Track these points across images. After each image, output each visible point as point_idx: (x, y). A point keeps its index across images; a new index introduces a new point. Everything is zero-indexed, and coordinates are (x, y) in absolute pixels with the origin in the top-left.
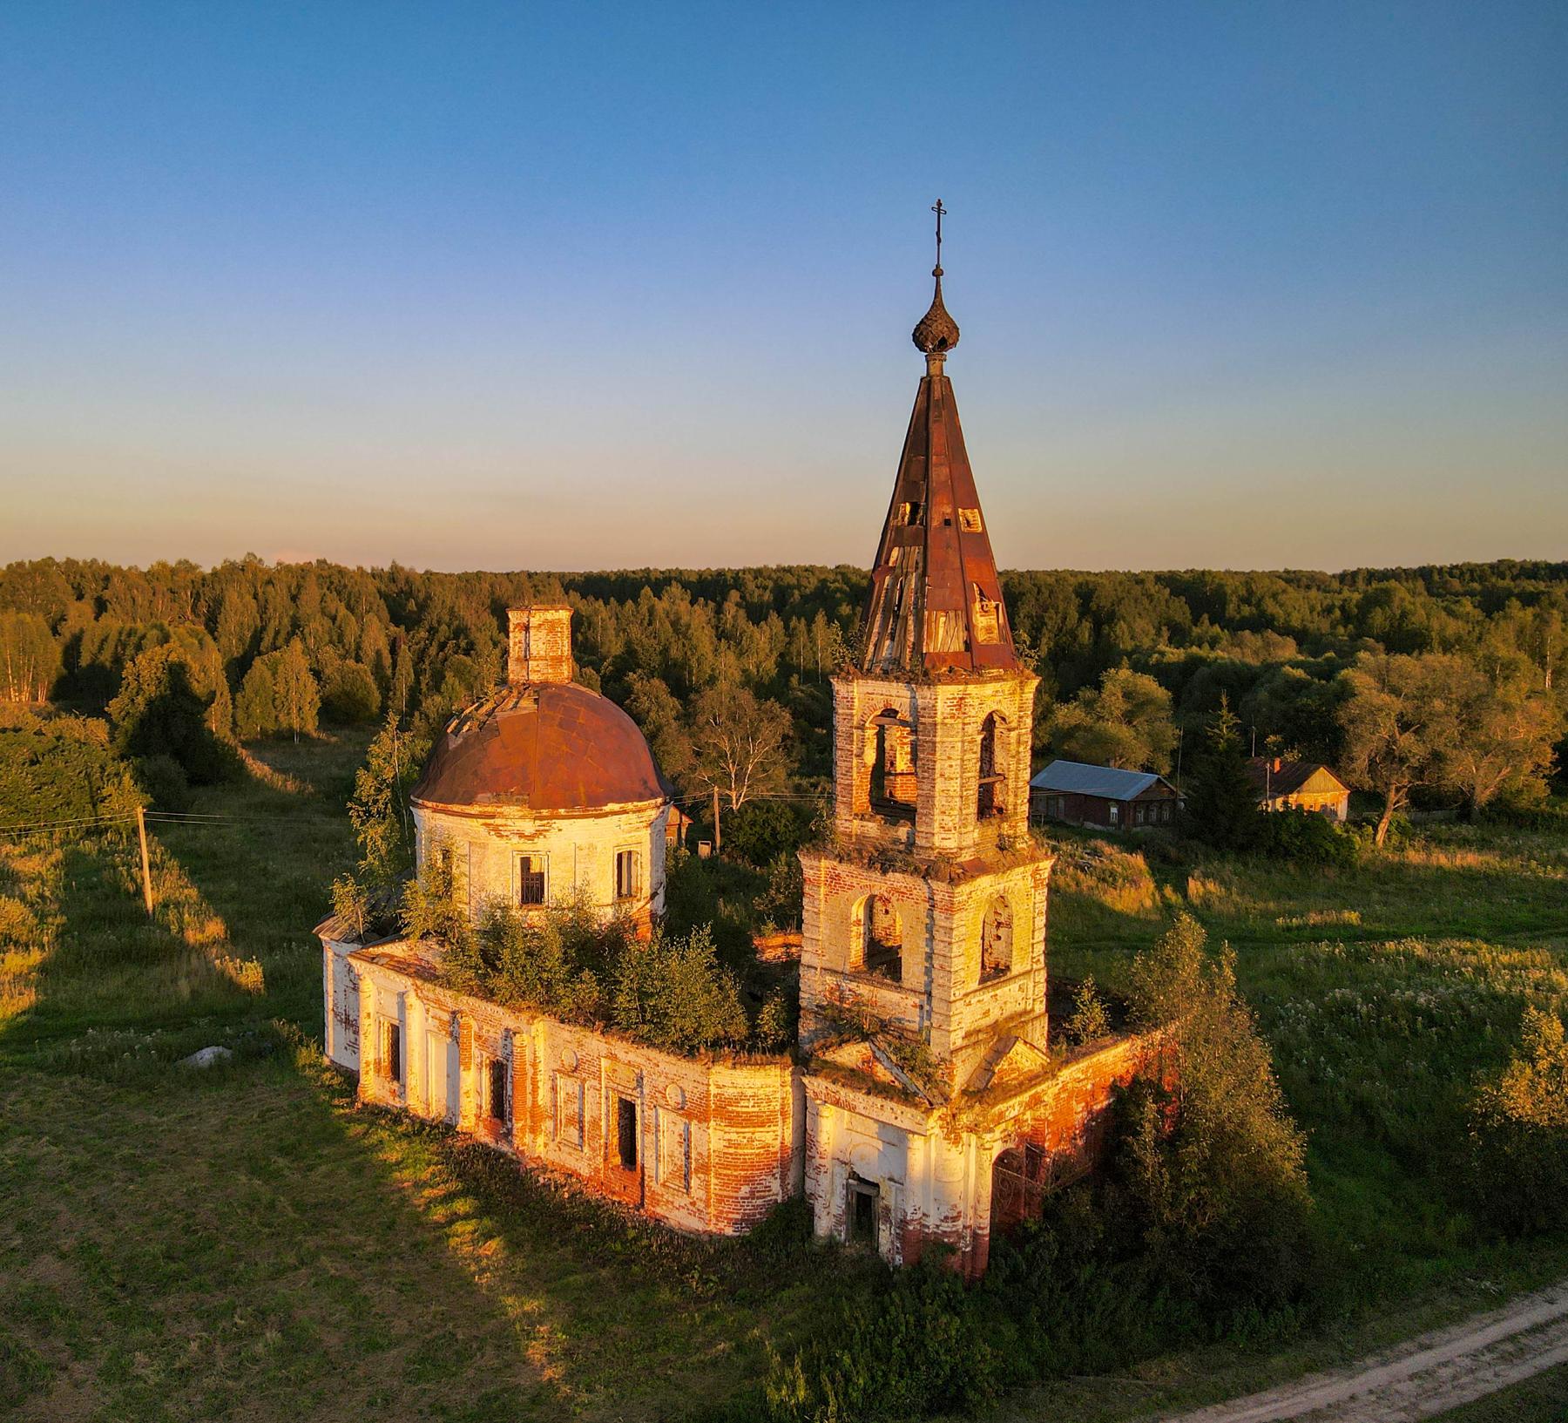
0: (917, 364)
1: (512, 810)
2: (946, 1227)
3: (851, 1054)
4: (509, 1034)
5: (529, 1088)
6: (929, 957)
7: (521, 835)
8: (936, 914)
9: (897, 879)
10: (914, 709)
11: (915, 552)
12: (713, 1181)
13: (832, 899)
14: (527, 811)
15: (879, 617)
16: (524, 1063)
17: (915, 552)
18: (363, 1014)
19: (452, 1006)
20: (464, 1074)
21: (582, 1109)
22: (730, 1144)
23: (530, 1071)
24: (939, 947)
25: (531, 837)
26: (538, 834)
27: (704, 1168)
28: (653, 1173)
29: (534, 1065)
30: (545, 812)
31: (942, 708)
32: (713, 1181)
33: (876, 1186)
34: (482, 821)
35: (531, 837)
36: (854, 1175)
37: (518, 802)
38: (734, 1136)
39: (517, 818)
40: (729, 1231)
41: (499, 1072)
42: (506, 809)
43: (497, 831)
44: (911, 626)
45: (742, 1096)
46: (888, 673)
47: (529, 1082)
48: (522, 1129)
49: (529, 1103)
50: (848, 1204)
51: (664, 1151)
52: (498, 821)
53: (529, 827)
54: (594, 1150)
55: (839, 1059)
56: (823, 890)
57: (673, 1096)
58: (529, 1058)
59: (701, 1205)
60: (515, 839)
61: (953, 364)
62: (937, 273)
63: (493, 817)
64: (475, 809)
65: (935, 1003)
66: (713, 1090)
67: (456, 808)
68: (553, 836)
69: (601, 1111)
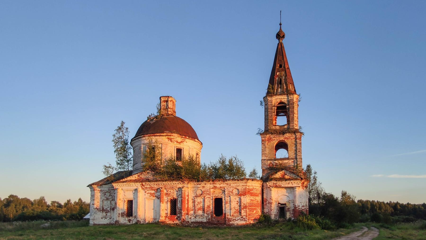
0: (277, 41)
1: (176, 135)
2: (303, 208)
3: (279, 175)
4: (180, 189)
5: (186, 202)
6: (296, 150)
7: (177, 142)
8: (297, 140)
9: (287, 135)
10: (289, 101)
11: (283, 73)
12: (248, 210)
13: (269, 144)
14: (179, 135)
15: (276, 85)
16: (185, 196)
17: (283, 73)
18: (118, 199)
19: (156, 187)
20: (162, 204)
21: (204, 205)
22: (252, 200)
23: (187, 198)
24: (298, 147)
25: (180, 143)
26: (182, 142)
27: (245, 207)
28: (229, 214)
29: (188, 196)
30: (184, 137)
31: (295, 100)
32: (248, 210)
33: (285, 204)
34: (167, 137)
35: (180, 143)
36: (279, 203)
37: (176, 133)
38: (252, 198)
39: (176, 137)
40: (252, 222)
41: (174, 202)
42: (173, 134)
43: (171, 140)
44: (285, 86)
45: (254, 189)
46: (282, 94)
47: (186, 200)
48: (185, 214)
49: (186, 206)
50: (278, 210)
51: (232, 207)
52: (172, 137)
53: (179, 139)
54: (208, 214)
55: (275, 177)
56: (267, 142)
57: (235, 191)
58: (186, 194)
59: (244, 217)
60: (176, 143)
61: (284, 41)
62: (280, 24)
63: (170, 136)
64: (165, 134)
65: (298, 159)
66: (247, 187)
67: (158, 134)
68: (185, 143)
69: (210, 203)
